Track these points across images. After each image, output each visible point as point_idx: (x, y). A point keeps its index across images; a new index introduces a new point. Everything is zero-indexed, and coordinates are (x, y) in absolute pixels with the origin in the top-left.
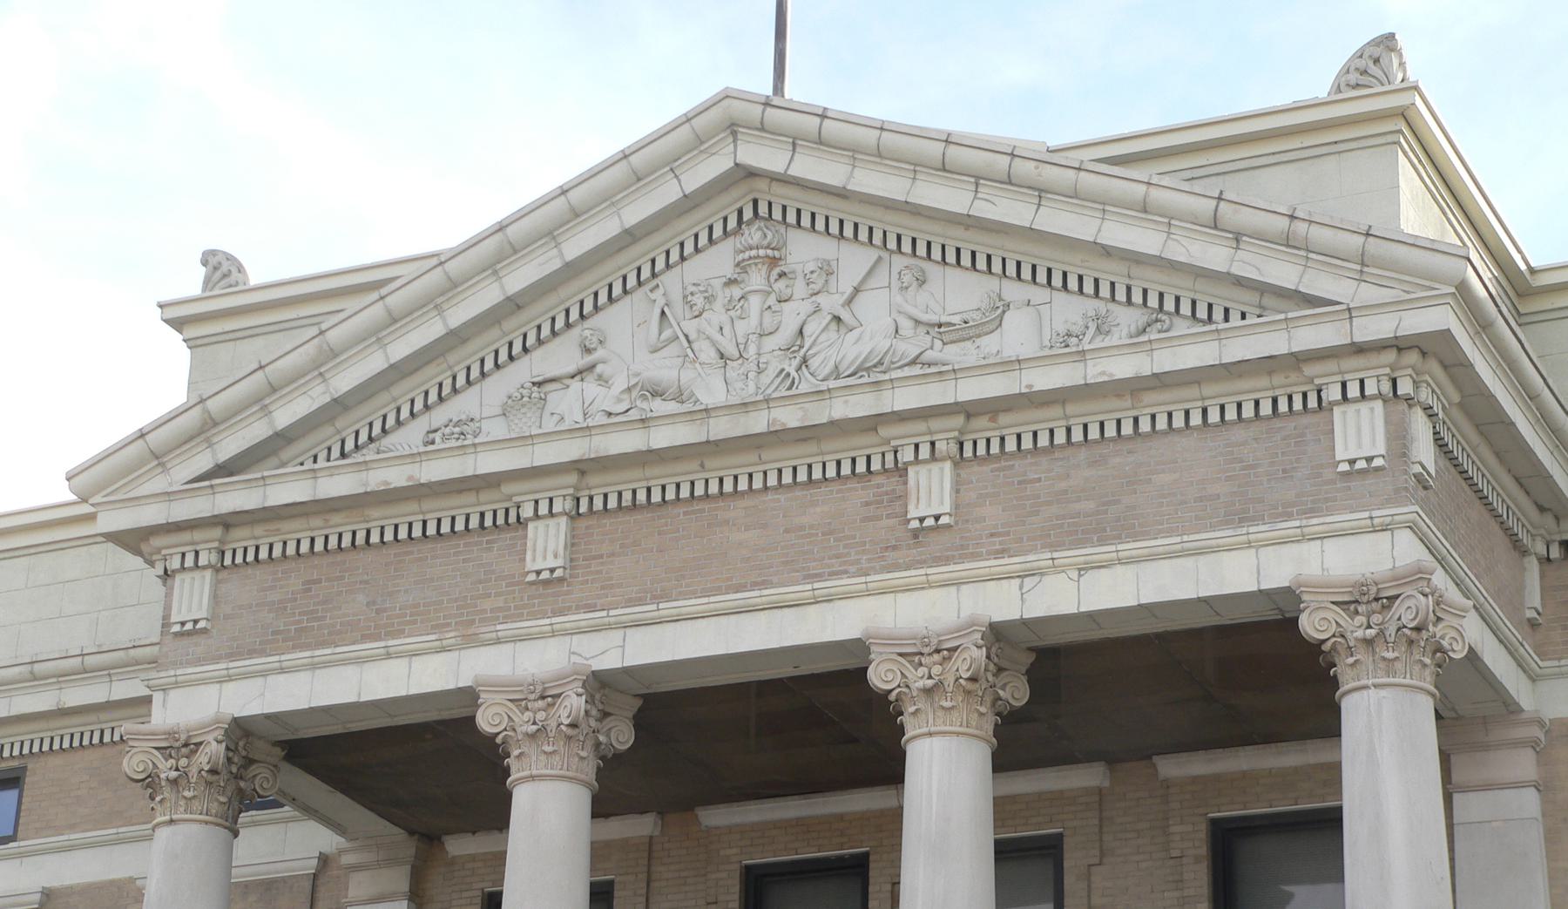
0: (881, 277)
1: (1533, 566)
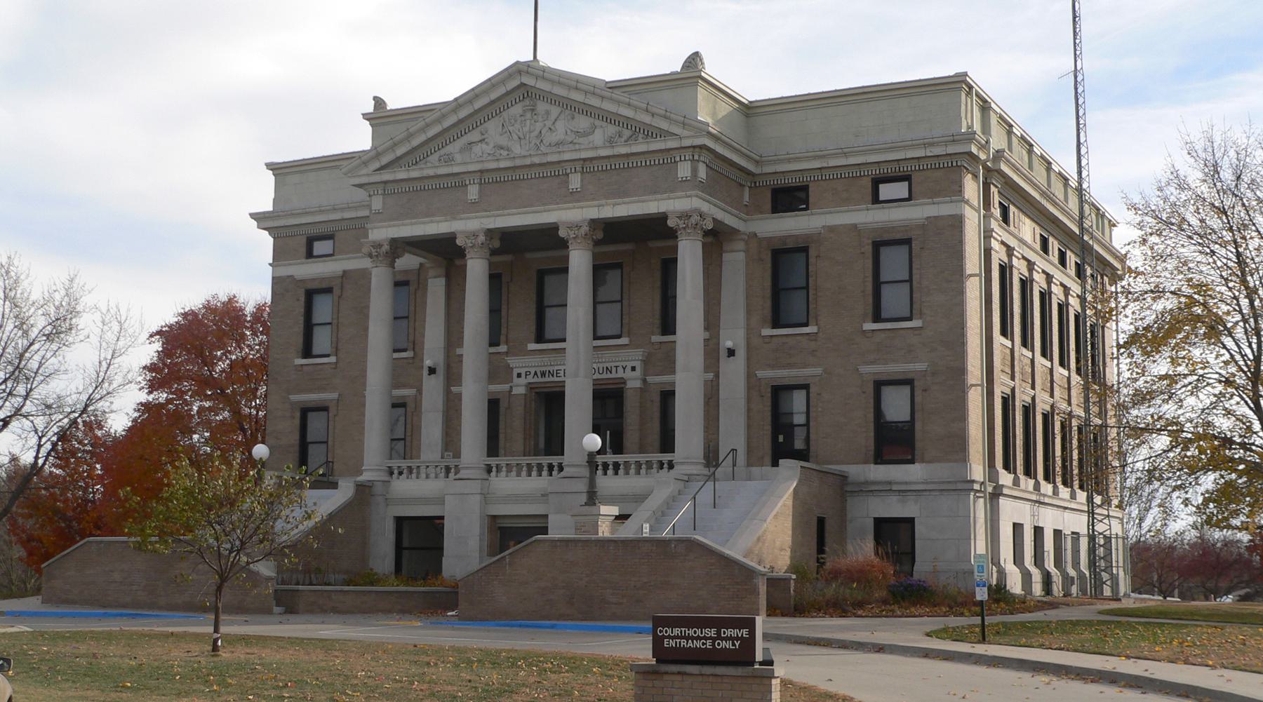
0: (562, 116)
1: (747, 189)
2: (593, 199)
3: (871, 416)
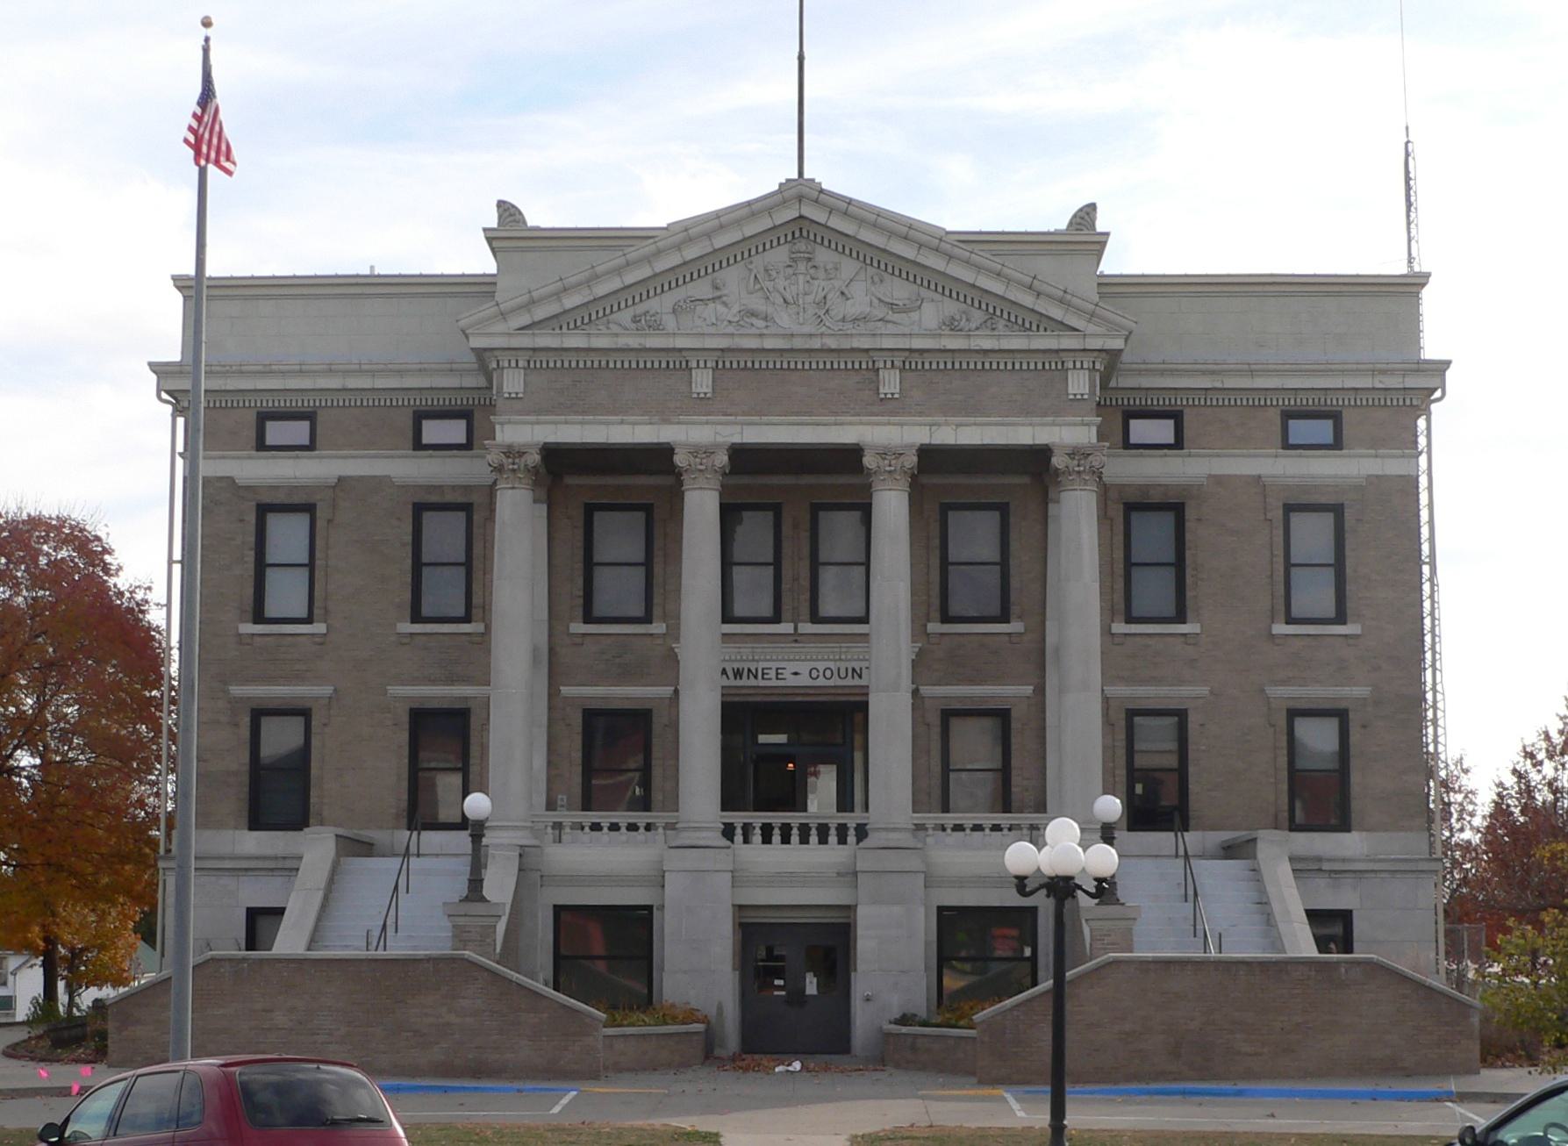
2: (921, 414)
3: (1283, 760)
